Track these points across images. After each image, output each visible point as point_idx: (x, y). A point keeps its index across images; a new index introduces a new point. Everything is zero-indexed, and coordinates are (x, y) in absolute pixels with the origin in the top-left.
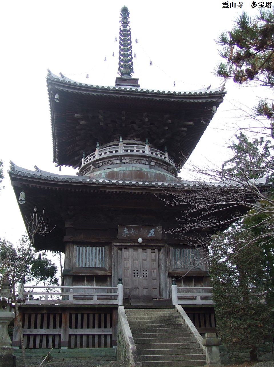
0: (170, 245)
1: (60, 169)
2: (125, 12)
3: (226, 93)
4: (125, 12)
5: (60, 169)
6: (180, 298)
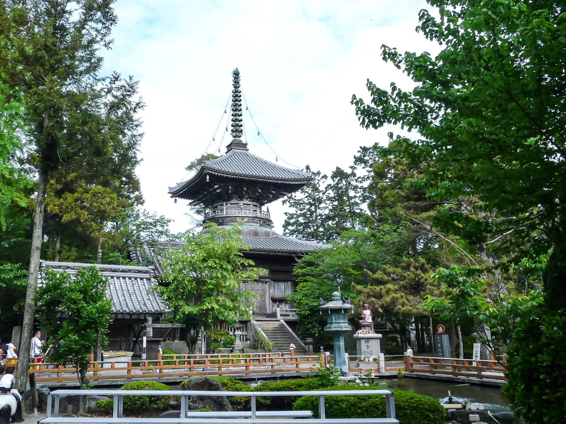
0: (272, 280)
1: (176, 201)
2: (236, 74)
3: (361, 147)
4: (236, 74)
5: (176, 201)
6: (281, 315)
